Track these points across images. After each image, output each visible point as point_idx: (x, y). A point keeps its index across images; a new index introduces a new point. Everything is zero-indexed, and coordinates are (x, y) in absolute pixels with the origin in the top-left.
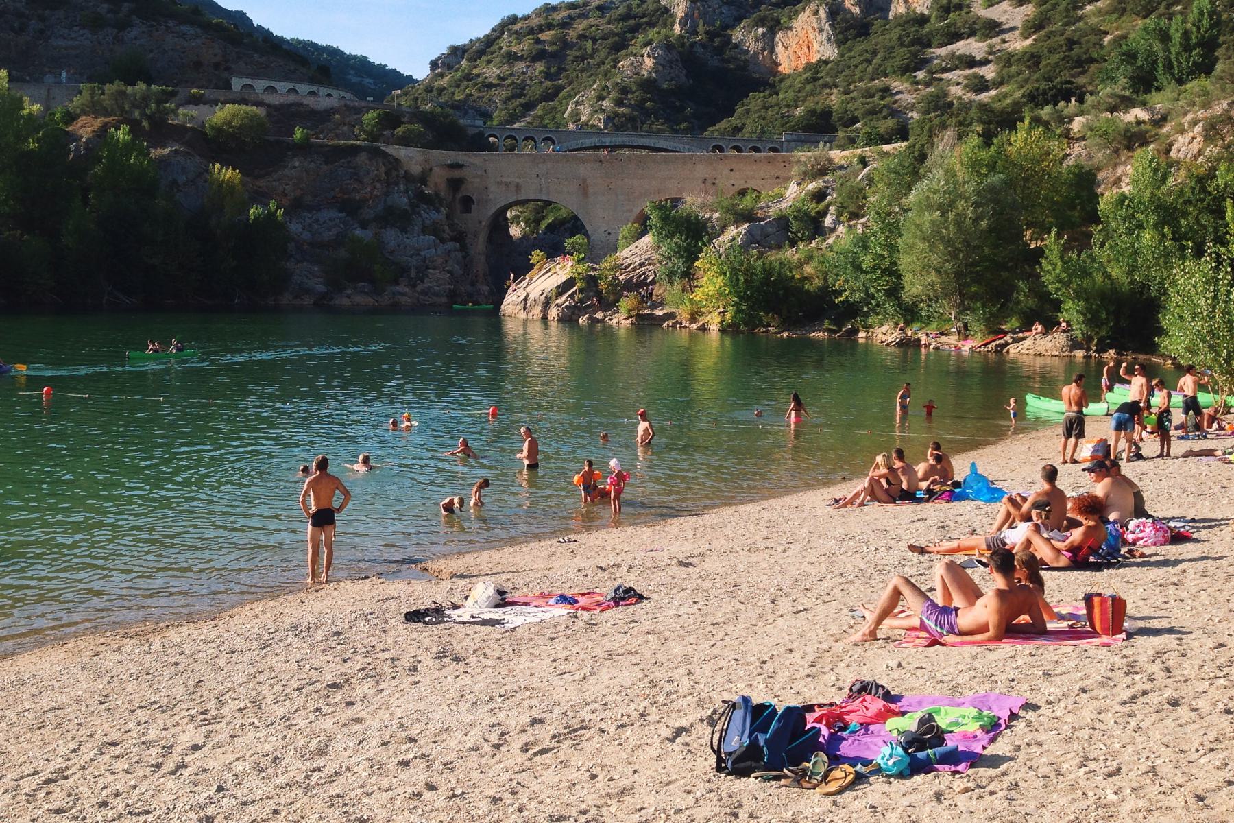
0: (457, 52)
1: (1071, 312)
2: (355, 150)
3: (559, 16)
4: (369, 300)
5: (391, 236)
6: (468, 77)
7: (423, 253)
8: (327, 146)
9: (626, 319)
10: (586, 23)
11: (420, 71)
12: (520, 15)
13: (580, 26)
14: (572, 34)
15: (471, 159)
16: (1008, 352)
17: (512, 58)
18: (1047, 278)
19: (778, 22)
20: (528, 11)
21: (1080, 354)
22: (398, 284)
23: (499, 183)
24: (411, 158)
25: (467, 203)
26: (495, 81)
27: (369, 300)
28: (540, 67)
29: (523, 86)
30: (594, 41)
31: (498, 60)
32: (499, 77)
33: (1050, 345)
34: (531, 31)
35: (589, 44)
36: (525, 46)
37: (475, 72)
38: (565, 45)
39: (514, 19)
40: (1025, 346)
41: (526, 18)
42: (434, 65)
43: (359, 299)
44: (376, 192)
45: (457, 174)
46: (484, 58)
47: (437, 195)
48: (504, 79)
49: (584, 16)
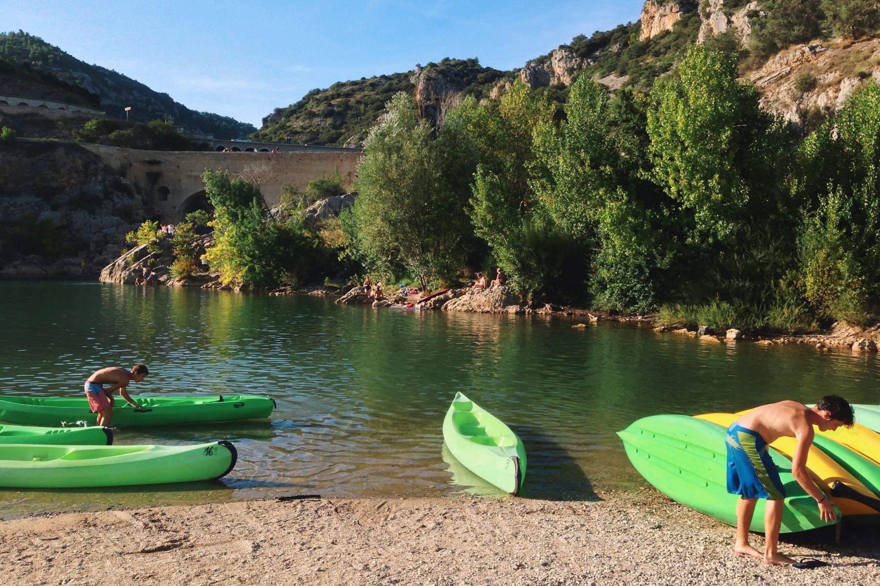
0: (279, 112)
1: (504, 258)
2: (53, 146)
3: (344, 90)
4: (37, 270)
5: (80, 217)
6: (283, 127)
7: (104, 231)
8: (29, 142)
9: (179, 281)
10: (363, 94)
11: (258, 125)
12: (321, 89)
13: (358, 96)
14: (352, 101)
15: (169, 158)
16: (446, 308)
17: (312, 115)
18: (476, 221)
19: (481, 92)
20: (327, 86)
21: (512, 309)
22: (77, 256)
23: (189, 177)
24: (111, 155)
25: (165, 192)
26: (299, 130)
27: (37, 270)
28: (329, 121)
29: (317, 133)
30: (366, 105)
31: (302, 117)
32: (302, 127)
33: (483, 299)
34: (326, 98)
35: (362, 107)
36: (322, 107)
37: (288, 124)
38: (347, 107)
39: (318, 91)
40: (461, 302)
41: (325, 91)
42: (265, 120)
43: (26, 269)
44: (73, 181)
45: (155, 169)
46: (295, 116)
47: (136, 185)
48: (305, 129)
49: (362, 90)
